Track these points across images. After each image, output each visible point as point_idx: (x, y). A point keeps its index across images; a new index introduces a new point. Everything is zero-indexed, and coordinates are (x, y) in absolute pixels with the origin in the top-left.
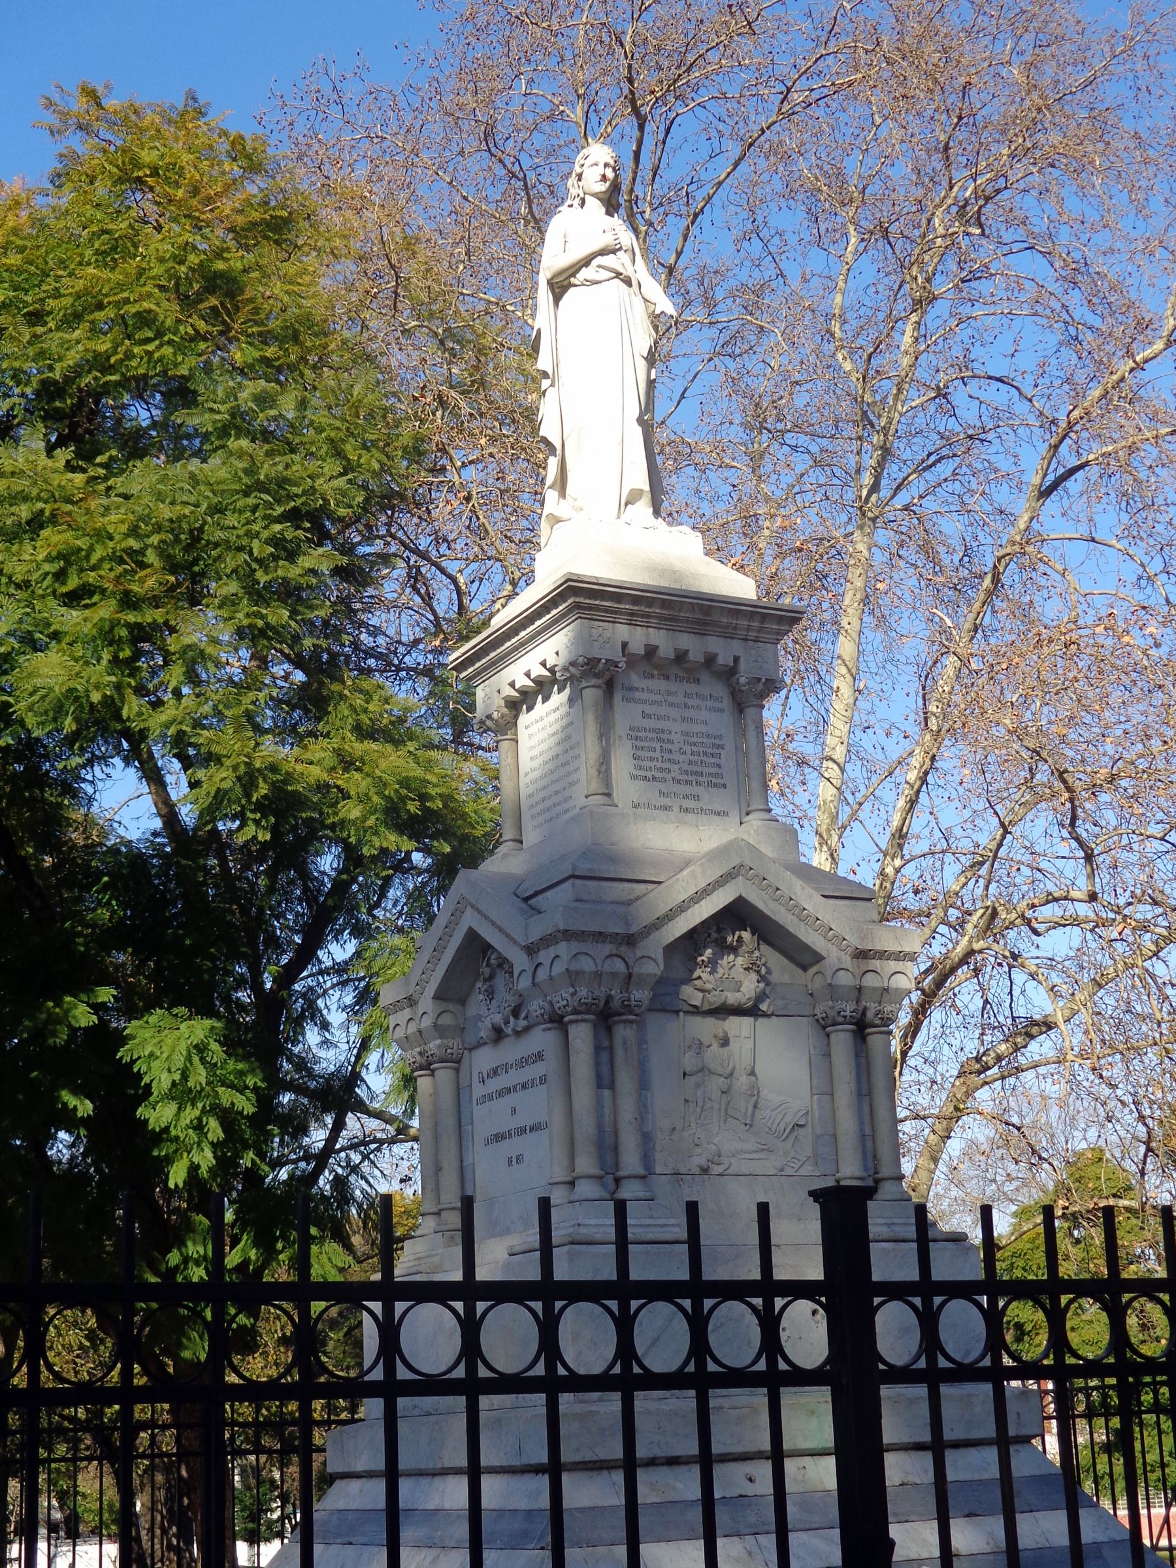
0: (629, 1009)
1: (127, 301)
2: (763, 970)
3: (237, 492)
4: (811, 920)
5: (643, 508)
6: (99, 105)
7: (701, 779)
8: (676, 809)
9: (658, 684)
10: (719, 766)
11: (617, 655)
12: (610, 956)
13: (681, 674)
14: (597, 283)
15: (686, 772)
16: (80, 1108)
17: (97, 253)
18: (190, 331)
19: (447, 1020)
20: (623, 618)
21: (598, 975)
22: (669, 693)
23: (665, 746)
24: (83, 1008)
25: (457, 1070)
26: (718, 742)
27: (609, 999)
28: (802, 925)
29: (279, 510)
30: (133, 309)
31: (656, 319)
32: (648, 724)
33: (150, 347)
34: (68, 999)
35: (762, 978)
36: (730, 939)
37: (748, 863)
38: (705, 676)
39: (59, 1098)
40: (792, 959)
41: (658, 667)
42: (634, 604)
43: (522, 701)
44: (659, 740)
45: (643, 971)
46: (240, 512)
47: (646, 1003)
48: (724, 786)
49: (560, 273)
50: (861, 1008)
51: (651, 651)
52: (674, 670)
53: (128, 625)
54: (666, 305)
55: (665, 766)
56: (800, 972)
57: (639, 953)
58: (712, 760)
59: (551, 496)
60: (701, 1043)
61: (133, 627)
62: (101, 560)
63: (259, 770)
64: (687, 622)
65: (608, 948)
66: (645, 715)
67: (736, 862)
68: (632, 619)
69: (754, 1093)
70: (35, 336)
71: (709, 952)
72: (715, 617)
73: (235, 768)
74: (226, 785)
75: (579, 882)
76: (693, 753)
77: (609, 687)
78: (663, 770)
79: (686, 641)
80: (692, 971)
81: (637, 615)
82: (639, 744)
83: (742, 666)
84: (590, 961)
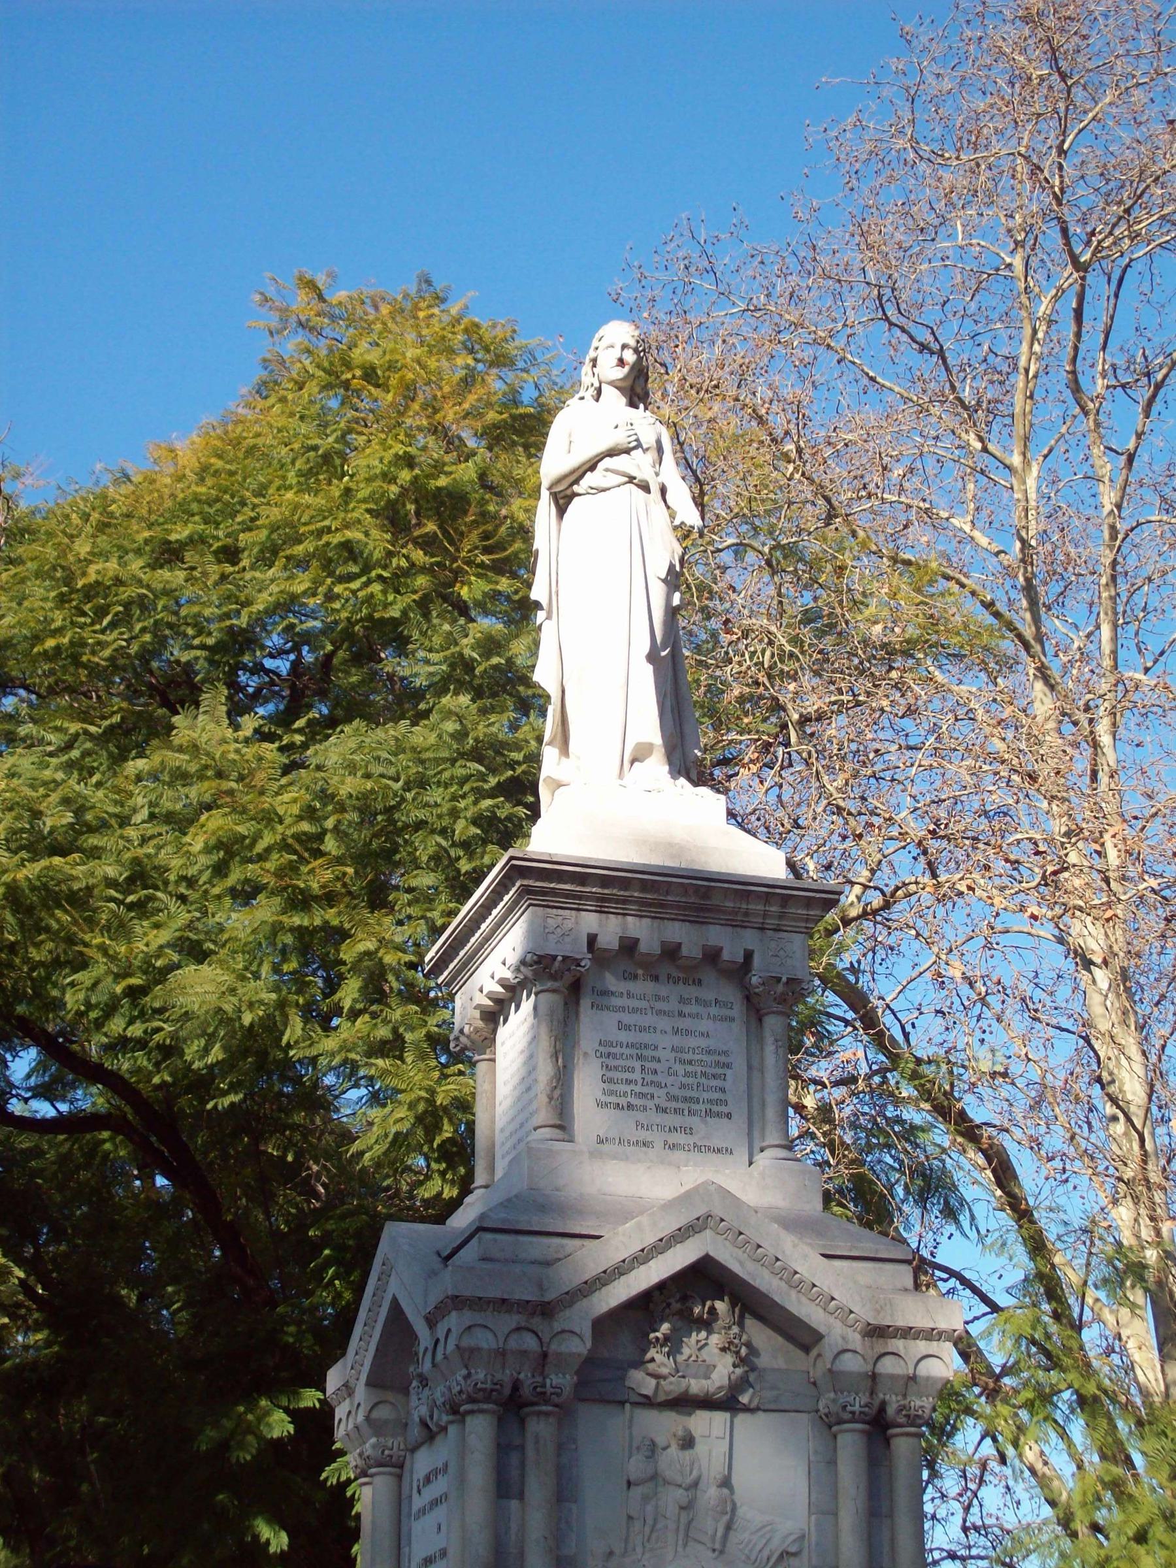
0: (542, 1397)
1: (328, 530)
2: (744, 1351)
3: (445, 760)
4: (806, 1286)
5: (657, 767)
6: (321, 298)
7: (694, 1107)
8: (659, 1144)
9: (643, 987)
10: (723, 1090)
11: (580, 950)
12: (518, 1329)
13: (675, 974)
14: (604, 490)
15: (675, 1098)
16: (273, 1542)
17: (300, 474)
18: (404, 563)
19: (383, 1413)
20: (591, 905)
21: (502, 1353)
22: (658, 998)
23: (648, 1065)
24: (279, 1416)
25: (400, 1477)
26: (723, 1059)
27: (516, 1386)
28: (793, 1293)
29: (493, 781)
30: (336, 539)
31: (684, 533)
32: (624, 1036)
33: (355, 585)
34: (263, 1403)
35: (742, 1361)
36: (697, 1310)
37: (718, 1212)
38: (709, 976)
39: (251, 1527)
40: (790, 1338)
41: (641, 965)
42: (603, 886)
43: (495, 1014)
44: (639, 1057)
45: (563, 1348)
46: (446, 786)
47: (568, 1391)
48: (729, 1116)
49: (559, 481)
50: (876, 1403)
51: (629, 946)
52: (665, 969)
53: (292, 930)
54: (690, 516)
55: (645, 1090)
56: (799, 1353)
57: (557, 1327)
58: (714, 1083)
59: (550, 754)
60: (653, 1444)
61: (299, 931)
62: (268, 850)
63: (445, 1109)
64: (679, 907)
65: (513, 1320)
66: (622, 1026)
67: (701, 1211)
68: (602, 906)
69: (729, 1511)
70: (224, 577)
71: (665, 1327)
72: (716, 901)
73: (412, 1106)
74: (404, 1127)
75: (489, 1236)
76: (687, 1074)
77: (575, 990)
78: (642, 1095)
79: (677, 932)
80: (645, 1351)
81: (609, 900)
82: (612, 1062)
83: (757, 961)
84: (490, 1336)
